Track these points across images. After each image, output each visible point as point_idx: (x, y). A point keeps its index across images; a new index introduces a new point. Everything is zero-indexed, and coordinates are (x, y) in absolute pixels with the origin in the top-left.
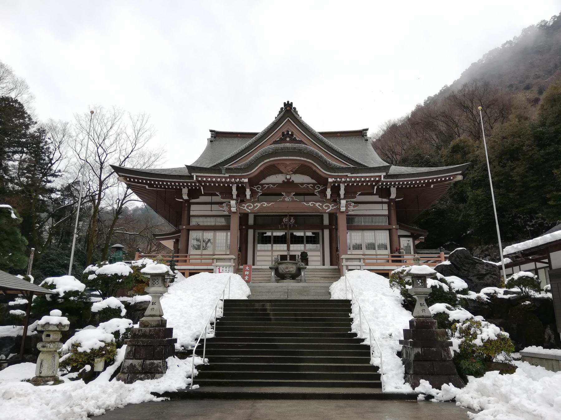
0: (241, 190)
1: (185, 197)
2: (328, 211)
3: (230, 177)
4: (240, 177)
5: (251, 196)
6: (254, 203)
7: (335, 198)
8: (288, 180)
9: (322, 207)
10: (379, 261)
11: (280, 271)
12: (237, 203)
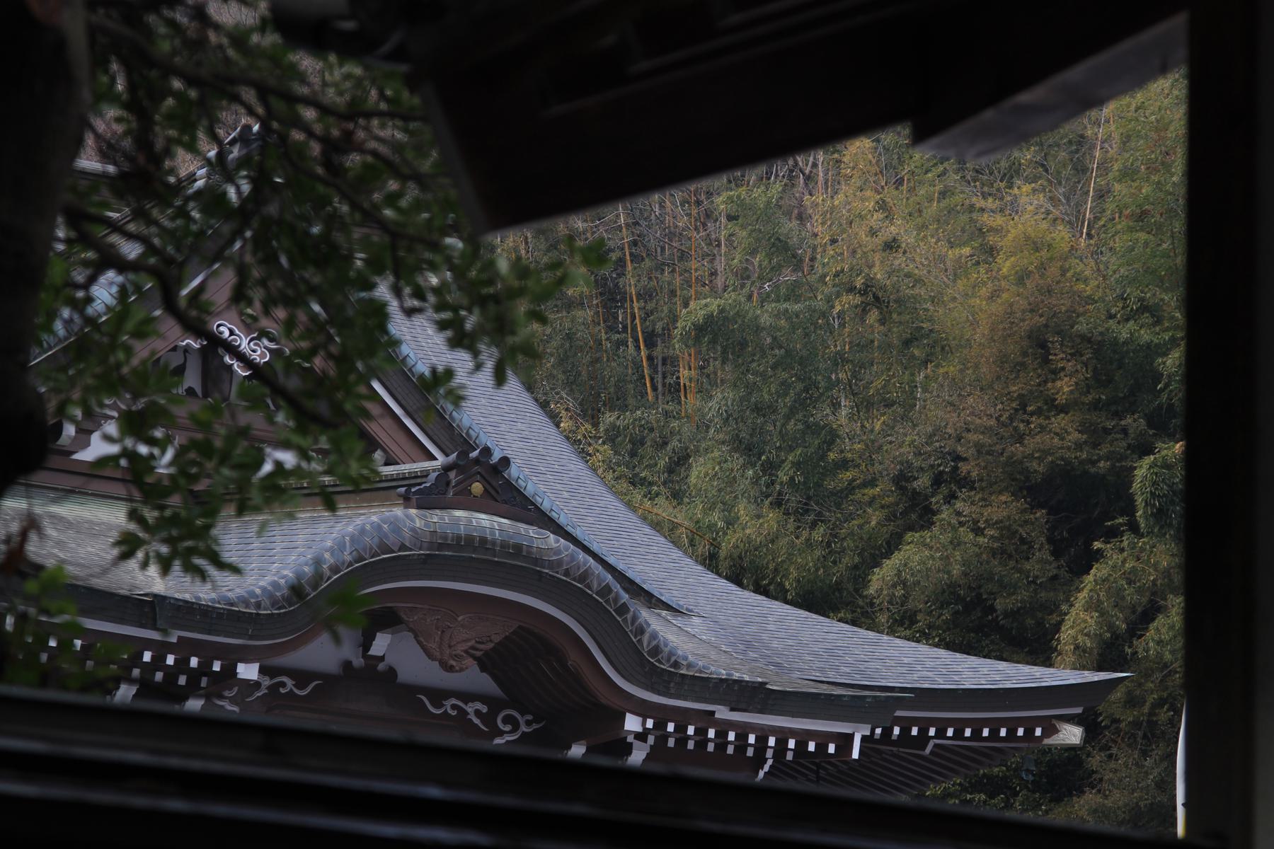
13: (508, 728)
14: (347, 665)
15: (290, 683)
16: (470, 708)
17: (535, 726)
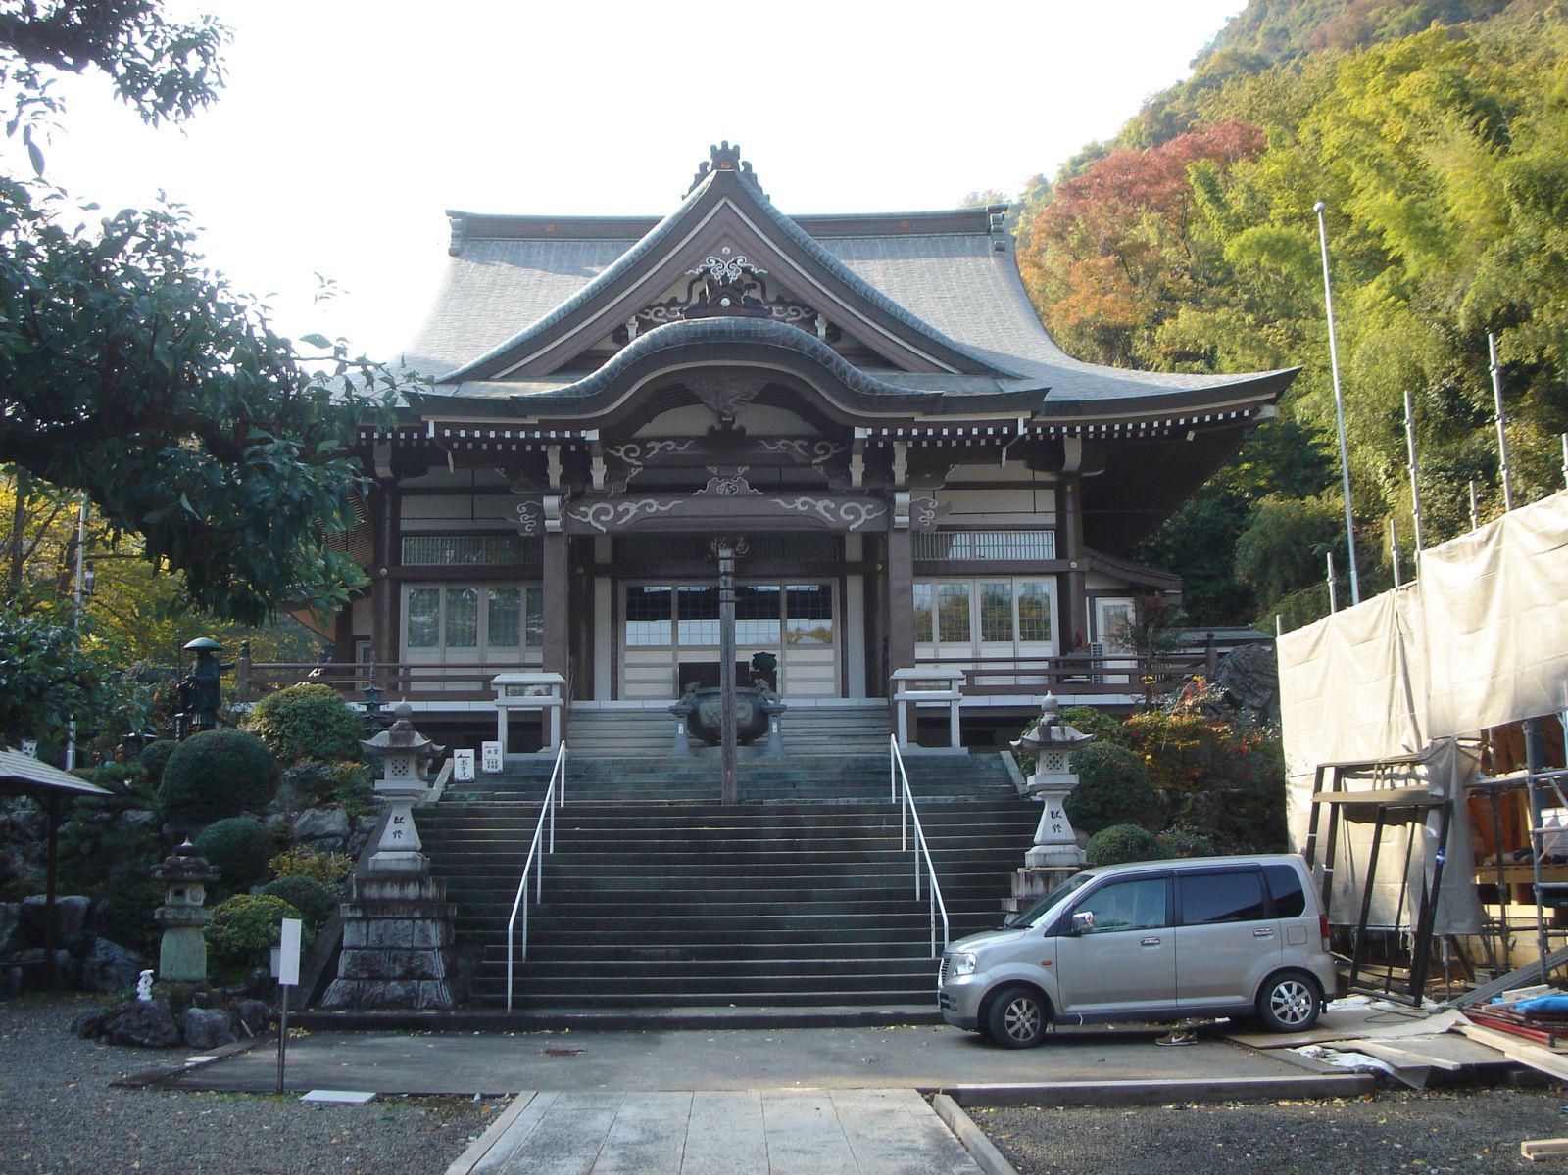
0: (577, 461)
2: (856, 525)
3: (544, 426)
5: (609, 478)
6: (617, 499)
7: (880, 489)
9: (834, 513)
11: (705, 720)
12: (562, 505)
15: (673, 445)
16: (796, 444)
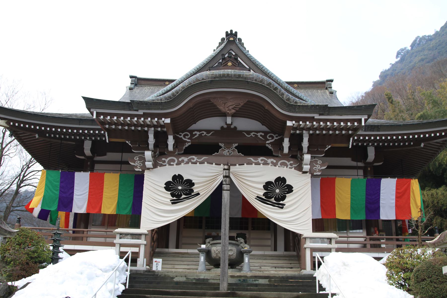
0: (161, 138)
1: (87, 151)
3: (145, 116)
4: (160, 116)
8: (229, 126)
10: (352, 246)
11: (214, 255)
12: (154, 156)
13: (270, 138)
14: (222, 127)
15: (205, 133)
16: (259, 134)
17: (279, 137)
